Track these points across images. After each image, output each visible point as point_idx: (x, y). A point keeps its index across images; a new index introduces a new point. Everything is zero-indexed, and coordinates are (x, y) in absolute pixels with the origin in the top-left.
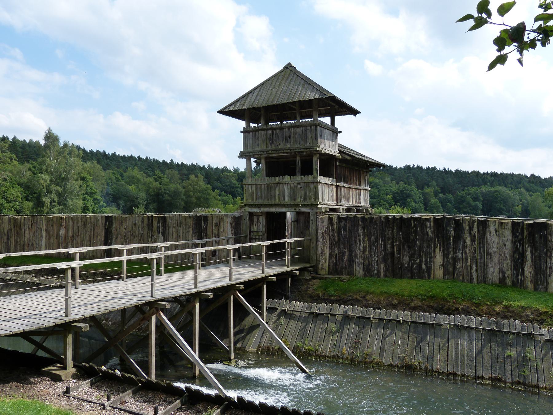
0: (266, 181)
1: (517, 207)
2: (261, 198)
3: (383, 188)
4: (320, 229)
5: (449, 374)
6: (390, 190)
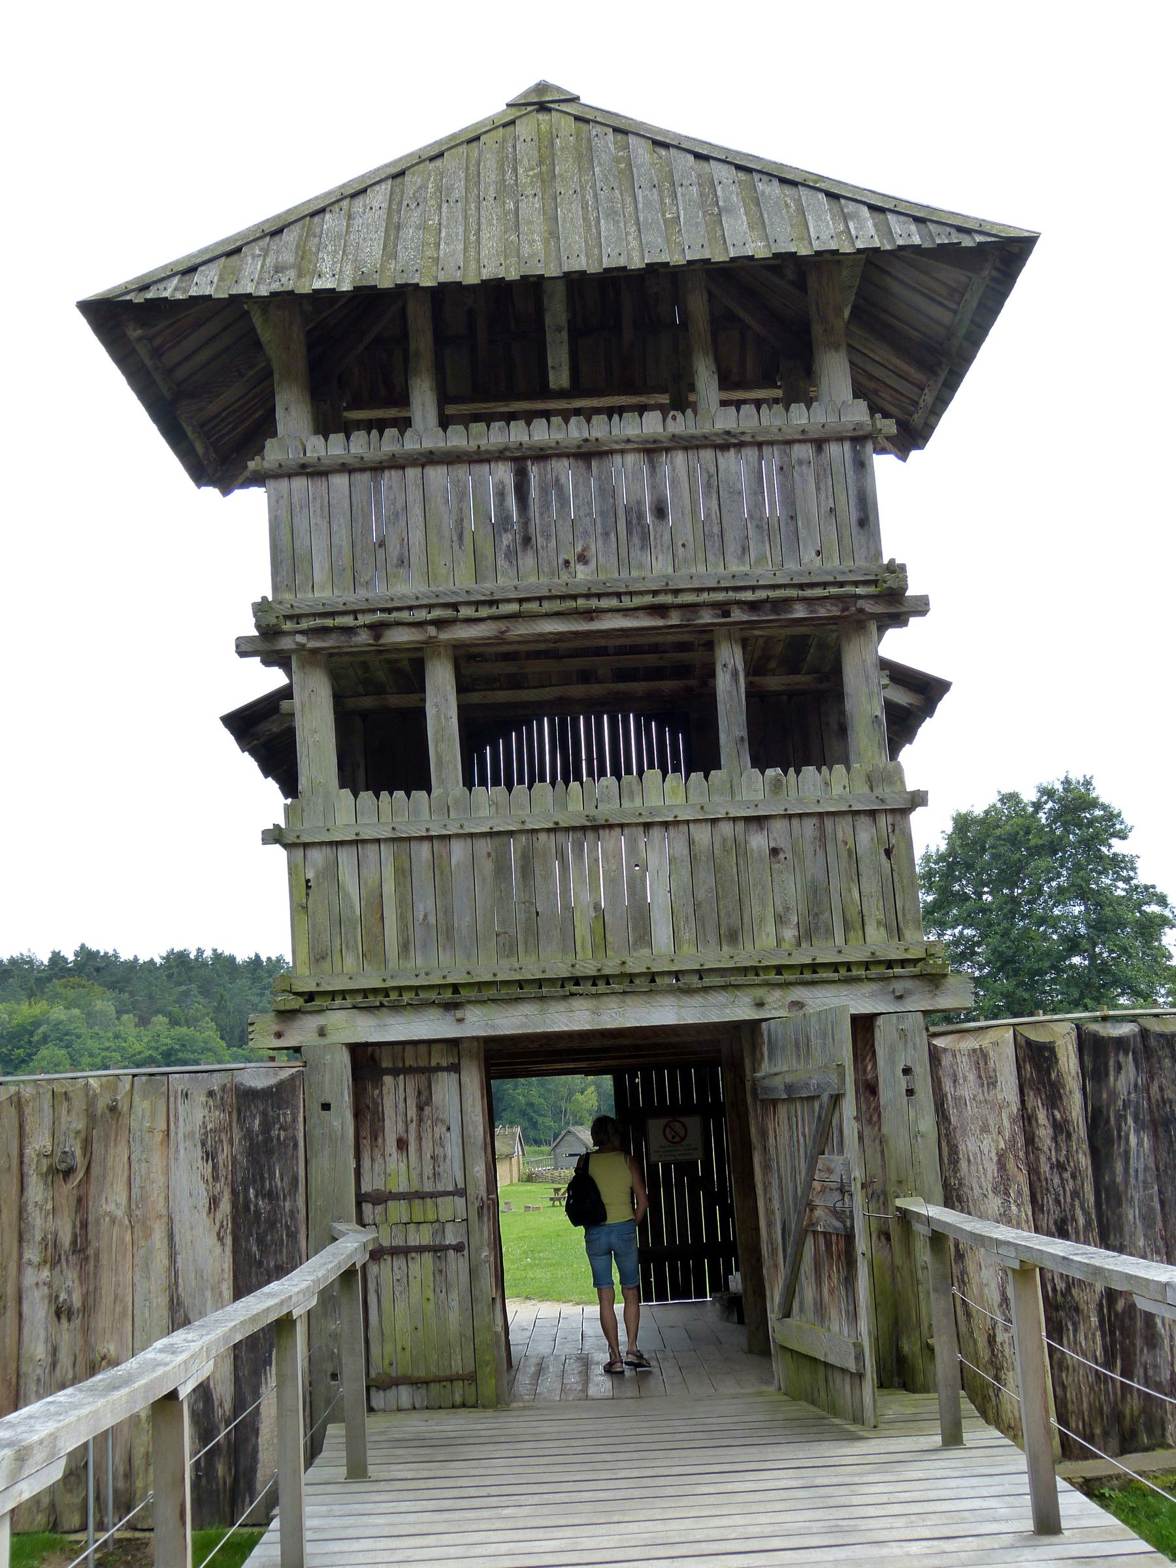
0: (485, 812)
1: (579, 1096)
2: (448, 934)
3: (90, 1043)
4: (974, 1127)
6: (120, 1049)
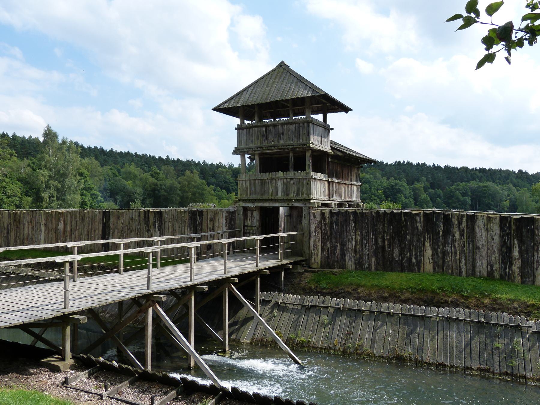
0: (260, 176)
1: (504, 202)
2: (255, 193)
3: (374, 183)
4: (312, 223)
5: (438, 365)
6: (381, 185)
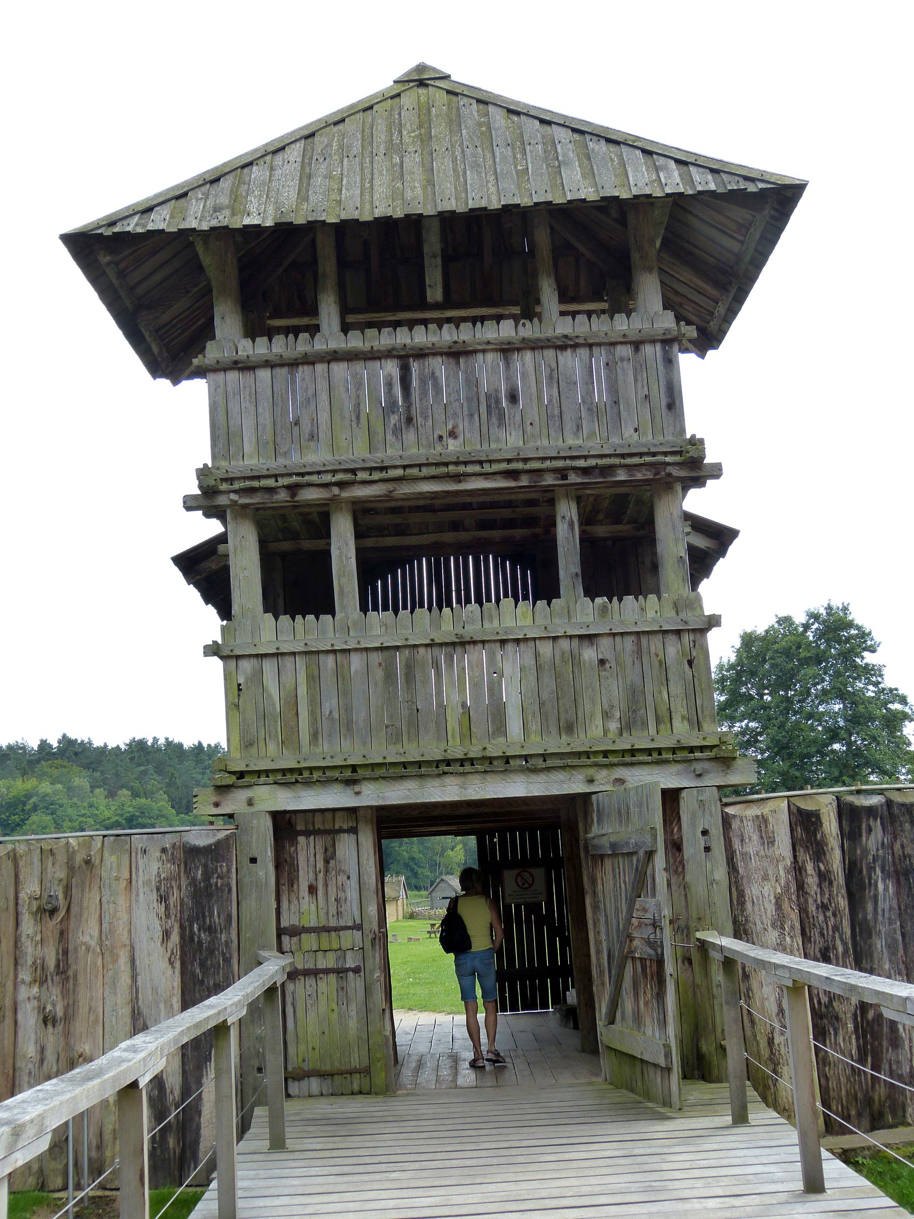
0: (377, 631)
1: (450, 852)
2: (348, 726)
3: (70, 811)
4: (757, 876)
6: (93, 815)
